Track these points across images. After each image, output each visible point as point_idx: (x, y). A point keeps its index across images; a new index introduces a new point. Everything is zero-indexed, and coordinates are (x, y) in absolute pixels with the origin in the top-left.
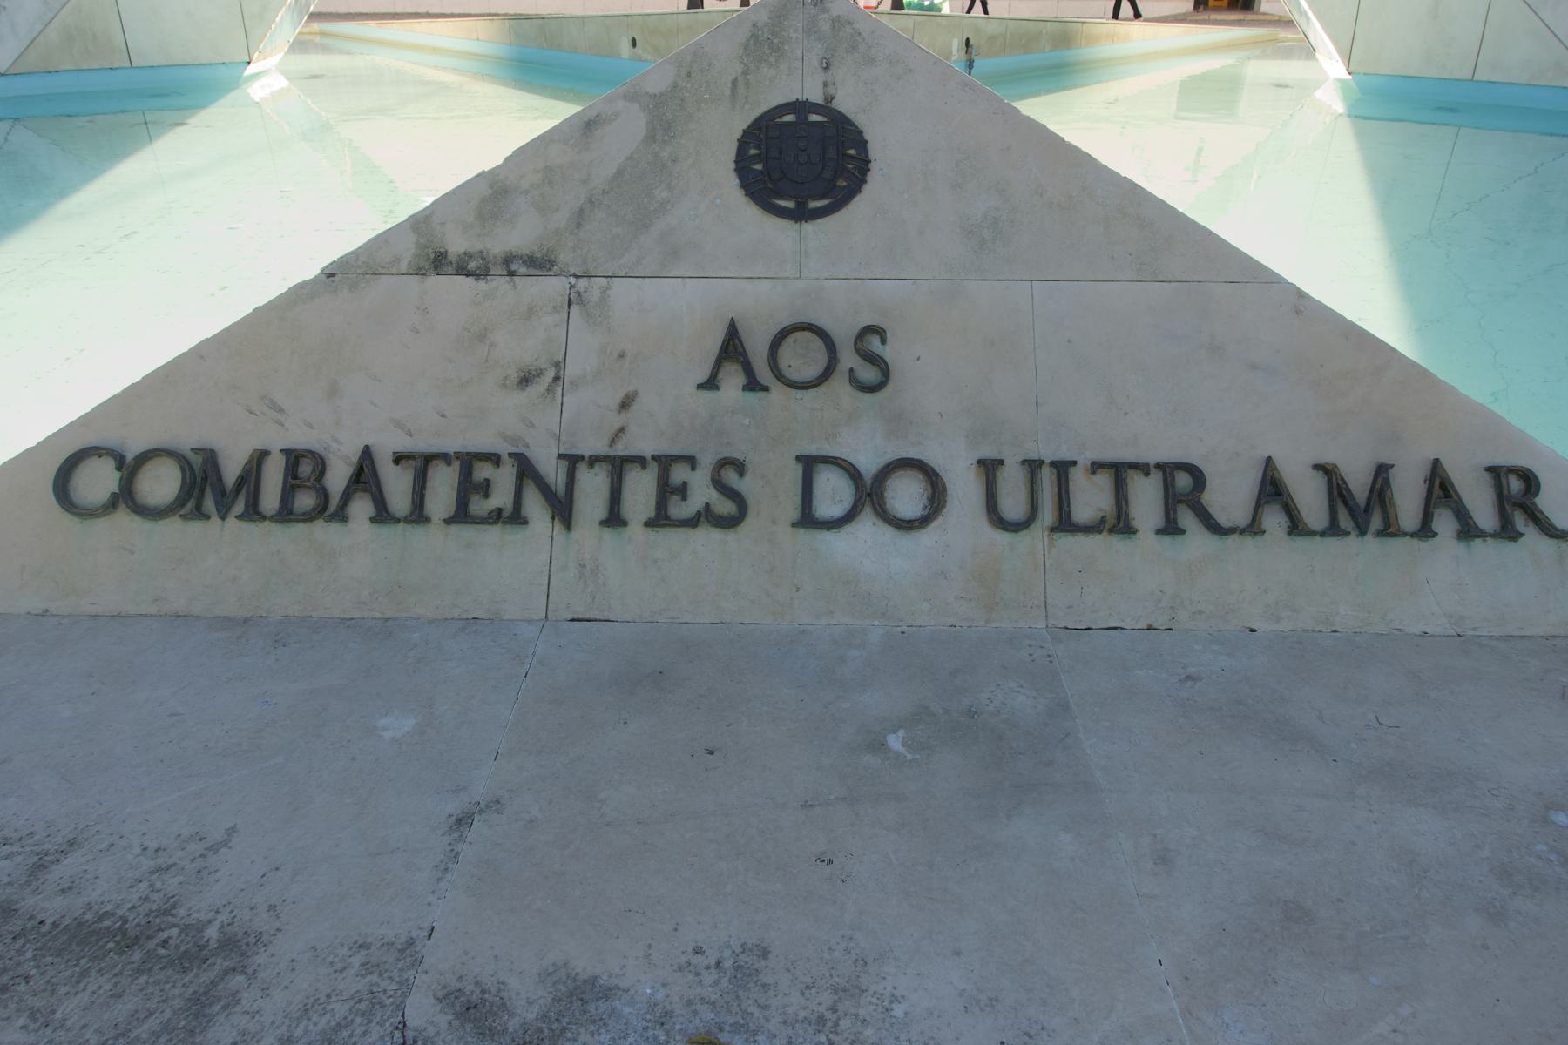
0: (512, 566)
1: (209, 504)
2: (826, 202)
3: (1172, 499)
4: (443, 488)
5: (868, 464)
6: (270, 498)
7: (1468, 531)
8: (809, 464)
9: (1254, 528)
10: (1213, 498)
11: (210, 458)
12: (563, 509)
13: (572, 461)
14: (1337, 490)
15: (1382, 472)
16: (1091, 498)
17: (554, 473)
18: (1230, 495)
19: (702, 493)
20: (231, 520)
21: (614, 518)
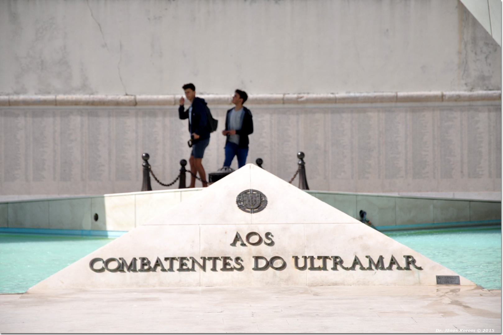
1: (125, 269)
3: (336, 264)
4: (176, 265)
6: (139, 266)
8: (257, 258)
12: (204, 267)
13: (204, 259)
14: (371, 261)
15: (381, 258)
16: (318, 263)
19: (233, 263)
21: (214, 269)
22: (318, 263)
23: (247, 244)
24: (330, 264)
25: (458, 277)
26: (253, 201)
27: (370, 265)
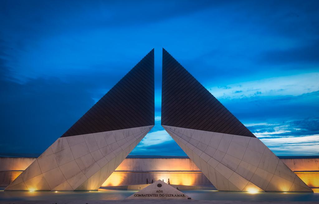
2: (280, 124)
8: (160, 195)
16: (169, 196)
22: (169, 196)
24: (171, 196)
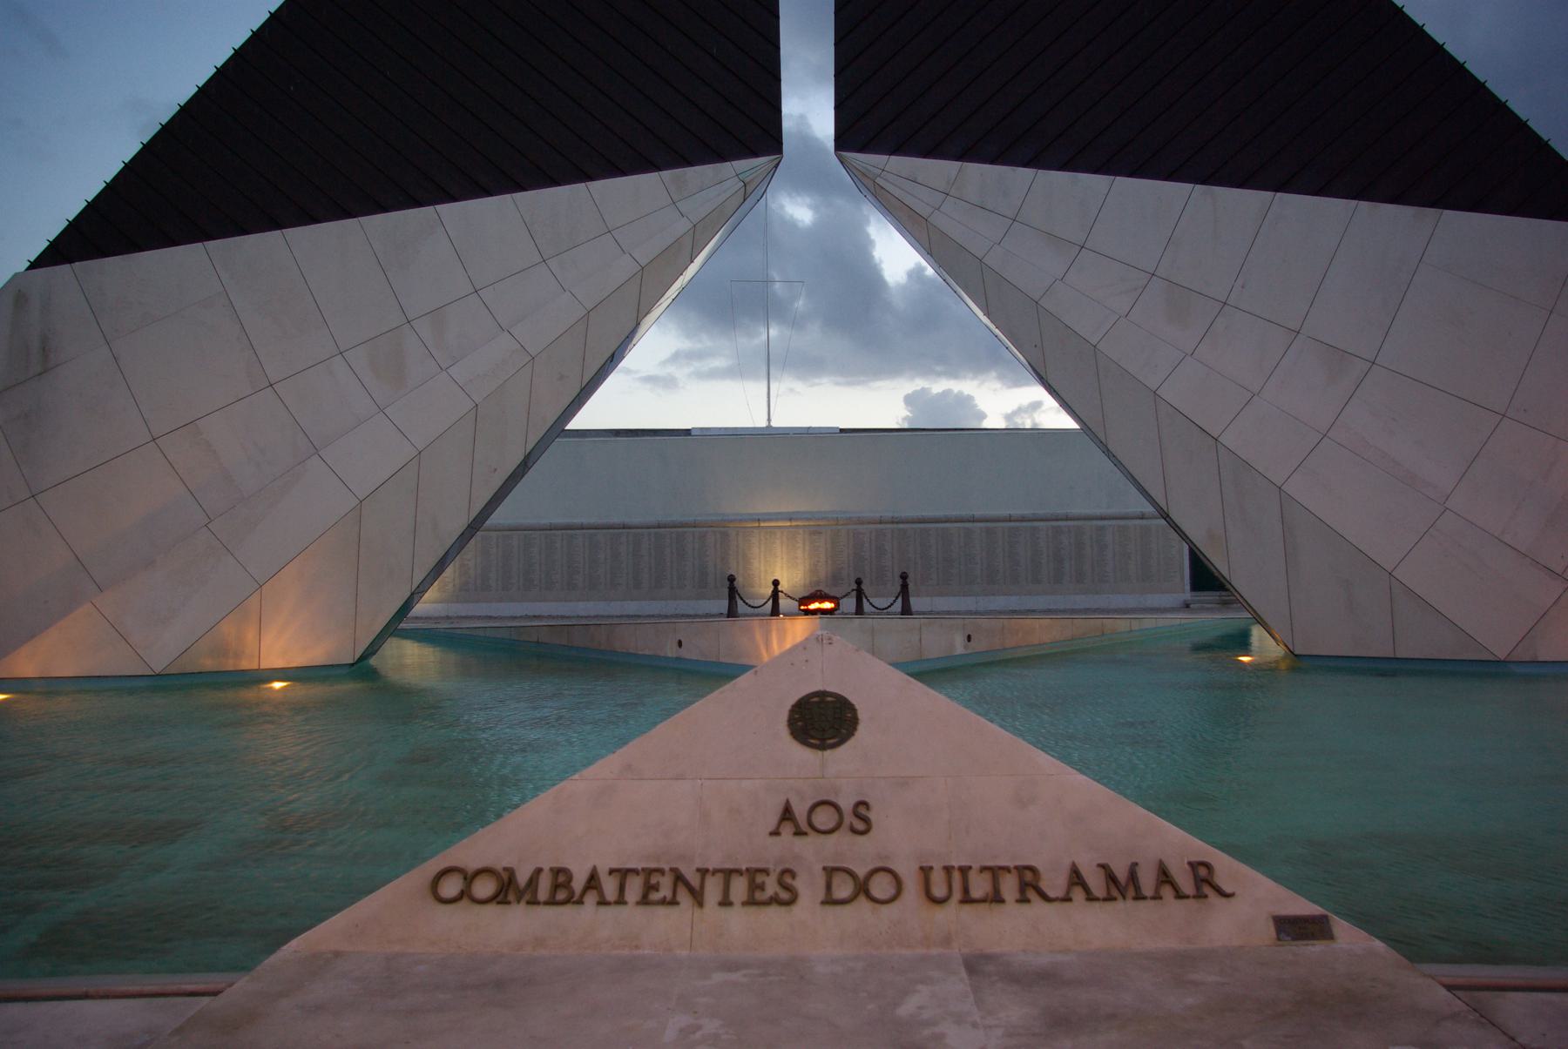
0: (667, 927)
1: (511, 897)
3: (1024, 886)
4: (634, 888)
5: (861, 872)
6: (543, 892)
7: (1180, 895)
8: (830, 872)
9: (1067, 899)
10: (1044, 885)
11: (511, 872)
12: (698, 896)
13: (703, 872)
14: (1111, 878)
17: (694, 880)
18: (1055, 883)
19: (772, 888)
20: (523, 903)
23: (808, 830)
25: (1325, 917)
26: (822, 720)
27: (1198, 888)
